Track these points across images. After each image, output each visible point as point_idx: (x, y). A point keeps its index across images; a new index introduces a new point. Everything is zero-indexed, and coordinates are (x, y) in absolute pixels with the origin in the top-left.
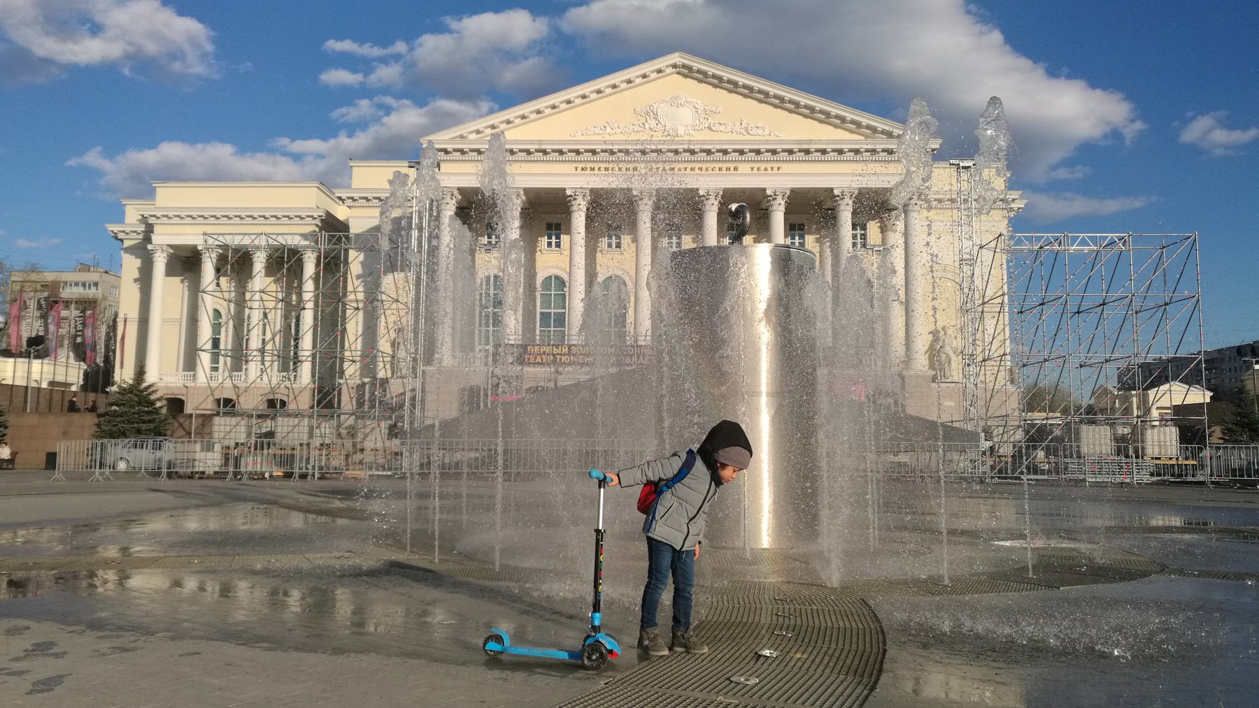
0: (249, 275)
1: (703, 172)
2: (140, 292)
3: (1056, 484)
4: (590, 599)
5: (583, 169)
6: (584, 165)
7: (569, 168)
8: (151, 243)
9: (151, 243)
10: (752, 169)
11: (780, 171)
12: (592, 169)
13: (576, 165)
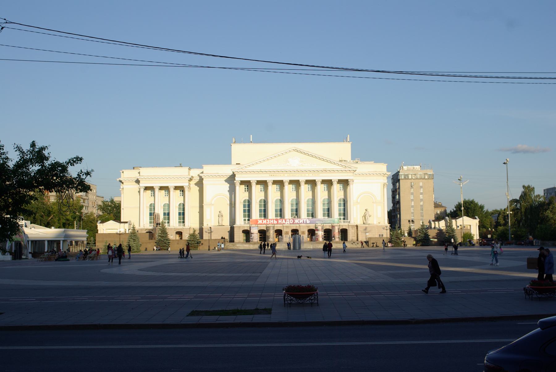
0: (267, 244)
1: (290, 176)
2: (230, 195)
3: (299, 252)
4: (208, 249)
5: (271, 175)
6: (273, 174)
7: (268, 175)
8: (235, 180)
9: (235, 180)
10: (313, 175)
11: (320, 175)
13: (313, 174)
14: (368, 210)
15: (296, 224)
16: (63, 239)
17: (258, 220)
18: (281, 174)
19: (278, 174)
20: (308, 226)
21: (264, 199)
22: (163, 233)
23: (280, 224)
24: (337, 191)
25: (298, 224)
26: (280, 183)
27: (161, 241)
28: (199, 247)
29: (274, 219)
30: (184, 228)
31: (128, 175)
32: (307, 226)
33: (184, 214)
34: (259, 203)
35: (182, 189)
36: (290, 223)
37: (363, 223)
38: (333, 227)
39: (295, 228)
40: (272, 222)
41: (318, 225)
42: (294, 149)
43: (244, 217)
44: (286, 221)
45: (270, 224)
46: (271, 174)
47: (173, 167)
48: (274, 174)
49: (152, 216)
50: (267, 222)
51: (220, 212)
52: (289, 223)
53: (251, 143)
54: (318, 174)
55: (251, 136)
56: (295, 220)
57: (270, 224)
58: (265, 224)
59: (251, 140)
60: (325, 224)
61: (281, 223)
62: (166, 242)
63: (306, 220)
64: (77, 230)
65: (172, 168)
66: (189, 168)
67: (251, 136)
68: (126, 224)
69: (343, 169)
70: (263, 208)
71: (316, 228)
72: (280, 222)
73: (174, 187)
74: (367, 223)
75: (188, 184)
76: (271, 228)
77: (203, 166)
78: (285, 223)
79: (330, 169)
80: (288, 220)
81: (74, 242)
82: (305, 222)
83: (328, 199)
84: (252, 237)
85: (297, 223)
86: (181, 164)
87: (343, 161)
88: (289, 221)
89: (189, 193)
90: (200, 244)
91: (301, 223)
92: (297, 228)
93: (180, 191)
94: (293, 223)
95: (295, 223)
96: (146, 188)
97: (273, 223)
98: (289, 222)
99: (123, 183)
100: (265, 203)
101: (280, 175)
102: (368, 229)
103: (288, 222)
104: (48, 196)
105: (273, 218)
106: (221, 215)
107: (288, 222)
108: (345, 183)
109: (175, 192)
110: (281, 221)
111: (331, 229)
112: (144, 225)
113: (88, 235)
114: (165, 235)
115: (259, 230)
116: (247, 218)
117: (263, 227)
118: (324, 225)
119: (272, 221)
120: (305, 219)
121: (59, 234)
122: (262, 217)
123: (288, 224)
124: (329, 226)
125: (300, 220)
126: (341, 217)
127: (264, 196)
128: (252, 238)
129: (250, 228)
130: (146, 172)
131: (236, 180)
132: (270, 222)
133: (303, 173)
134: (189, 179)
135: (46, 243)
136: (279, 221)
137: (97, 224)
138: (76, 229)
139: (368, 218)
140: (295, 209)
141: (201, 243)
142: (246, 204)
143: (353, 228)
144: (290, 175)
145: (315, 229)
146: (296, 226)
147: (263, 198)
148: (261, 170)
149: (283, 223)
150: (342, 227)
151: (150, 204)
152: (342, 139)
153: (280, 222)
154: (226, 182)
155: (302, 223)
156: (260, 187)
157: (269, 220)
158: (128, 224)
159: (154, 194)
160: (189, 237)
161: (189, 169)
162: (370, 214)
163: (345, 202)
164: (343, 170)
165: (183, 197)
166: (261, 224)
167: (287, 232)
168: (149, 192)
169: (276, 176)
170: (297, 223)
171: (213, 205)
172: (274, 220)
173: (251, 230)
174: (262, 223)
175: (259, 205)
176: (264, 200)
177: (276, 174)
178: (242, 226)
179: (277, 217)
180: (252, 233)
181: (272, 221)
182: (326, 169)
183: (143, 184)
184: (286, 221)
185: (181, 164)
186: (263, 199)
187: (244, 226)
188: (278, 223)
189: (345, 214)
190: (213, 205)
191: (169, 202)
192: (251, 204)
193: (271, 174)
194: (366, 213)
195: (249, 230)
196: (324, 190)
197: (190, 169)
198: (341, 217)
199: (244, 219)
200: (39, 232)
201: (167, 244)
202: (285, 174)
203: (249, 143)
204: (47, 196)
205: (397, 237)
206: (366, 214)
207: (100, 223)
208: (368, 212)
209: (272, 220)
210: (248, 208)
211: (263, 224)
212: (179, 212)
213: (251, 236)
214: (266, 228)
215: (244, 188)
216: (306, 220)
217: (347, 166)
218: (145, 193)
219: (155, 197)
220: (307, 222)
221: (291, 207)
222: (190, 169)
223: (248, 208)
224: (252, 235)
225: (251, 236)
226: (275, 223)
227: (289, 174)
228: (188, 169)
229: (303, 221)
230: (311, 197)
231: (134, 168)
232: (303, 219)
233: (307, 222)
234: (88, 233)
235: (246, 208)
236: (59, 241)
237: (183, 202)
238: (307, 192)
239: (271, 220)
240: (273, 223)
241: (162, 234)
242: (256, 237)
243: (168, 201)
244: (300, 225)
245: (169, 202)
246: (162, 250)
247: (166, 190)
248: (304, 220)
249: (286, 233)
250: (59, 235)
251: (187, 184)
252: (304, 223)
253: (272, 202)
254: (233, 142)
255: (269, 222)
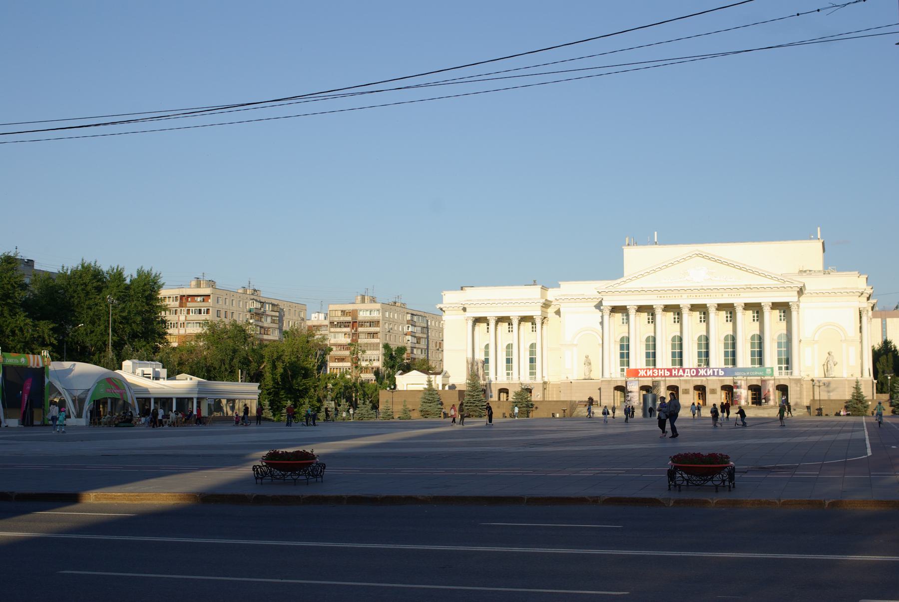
1: (691, 297)
8: (602, 306)
9: (602, 306)
12: (696, 296)
14: (833, 354)
15: (701, 376)
16: (196, 396)
17: (640, 371)
18: (683, 295)
19: (671, 295)
20: (722, 381)
21: (758, 333)
22: (475, 391)
23: (675, 376)
24: (773, 322)
25: (704, 376)
26: (729, 309)
27: (471, 403)
28: (531, 413)
29: (664, 369)
30: (791, 377)
31: (451, 298)
32: (719, 380)
33: (654, 354)
34: (671, 342)
35: (704, 310)
36: (691, 375)
37: (824, 376)
38: (763, 381)
39: (699, 384)
40: (661, 374)
41: (737, 378)
42: (697, 253)
43: (621, 366)
44: (684, 372)
45: (658, 376)
46: (659, 296)
47: (521, 285)
48: (666, 295)
49: (511, 364)
50: (653, 373)
51: (829, 353)
52: (689, 374)
53: (656, 244)
54: (738, 294)
55: (656, 233)
56: (700, 370)
57: (658, 376)
58: (650, 376)
59: (656, 241)
60: (751, 376)
61: (676, 375)
62: (478, 405)
63: (717, 370)
64: (242, 383)
65: (520, 287)
66: (543, 286)
67: (656, 233)
68: (438, 376)
69: (779, 284)
70: (730, 350)
71: (735, 383)
72: (675, 374)
73: (663, 307)
74: (830, 375)
75: (540, 312)
76: (662, 384)
77: (560, 283)
78: (683, 375)
79: (758, 285)
80: (689, 370)
81: (224, 402)
82: (716, 374)
83: (787, 335)
84: (629, 398)
85: (642, 375)
86: (535, 281)
87: (808, 272)
88: (689, 372)
89: (690, 317)
90: (534, 409)
91: (710, 375)
92: (703, 384)
93: (700, 313)
94: (697, 375)
95: (699, 374)
96: (615, 309)
97: (663, 375)
98: (690, 373)
99: (444, 311)
100: (759, 342)
101: (716, 296)
102: (833, 386)
103: (687, 373)
104: (356, 334)
105: (664, 368)
106: (588, 363)
107: (687, 373)
108: (784, 308)
109: (525, 326)
110: (676, 372)
111: (760, 385)
112: (611, 374)
113: (260, 391)
114: (476, 393)
115: (640, 386)
116: (784, 366)
117: (648, 382)
118: (748, 378)
119: (661, 371)
120: (716, 368)
121: (191, 389)
122: (755, 364)
123: (687, 376)
124: (757, 380)
125: (708, 370)
126: (509, 372)
127: (732, 329)
128: (629, 399)
129: (626, 382)
130: (473, 294)
131: (603, 305)
132: (658, 372)
133: (713, 293)
134: (542, 305)
135: (152, 401)
136: (673, 372)
137: (395, 376)
138: (241, 381)
139: (831, 367)
140: (704, 351)
141: (535, 406)
142: (728, 343)
143: (797, 384)
144: (690, 296)
145: (732, 385)
146: (702, 380)
147: (758, 333)
148: (702, 286)
149: (679, 375)
150: (779, 381)
151: (646, 337)
152: (804, 234)
153: (675, 374)
154: (596, 309)
155: (712, 374)
156: (726, 315)
157: (657, 371)
158: (442, 376)
159: (628, 319)
160: (514, 397)
161: (541, 288)
162: (836, 359)
163: (788, 341)
164: (779, 286)
165: (731, 323)
166: (644, 376)
167: (686, 390)
168: (619, 316)
169: (668, 298)
170: (702, 375)
171: (576, 345)
172: (666, 370)
173: (628, 387)
174: (645, 375)
175: (750, 344)
176: (705, 337)
177: (668, 295)
178: (613, 379)
179: (727, 365)
180: (629, 392)
181: (661, 371)
182: (750, 285)
183: (608, 303)
184: (684, 372)
185: (535, 281)
186: (757, 335)
187: (617, 380)
188: (671, 375)
189: (787, 362)
190: (576, 345)
191: (655, 333)
192: (764, 343)
193: (659, 296)
194: (828, 360)
195: (625, 386)
196: (779, 320)
197: (544, 288)
198: (509, 372)
199: (779, 367)
200: (164, 385)
201: (480, 407)
202: (682, 295)
203: (653, 244)
204: (354, 334)
205: (857, 400)
206: (828, 361)
207: (401, 374)
208: (832, 356)
209: (661, 369)
210: (732, 350)
211: (647, 377)
212: (507, 359)
213: (628, 396)
214: (653, 383)
215: (699, 316)
216: (717, 370)
217: (785, 280)
218: (638, 318)
219: (629, 325)
220: (720, 374)
221: (646, 350)
222: (544, 288)
223: (732, 350)
224: (630, 394)
225: (628, 396)
226: (666, 375)
227: (689, 295)
228: (540, 289)
229: (714, 372)
230: (785, 332)
231: (462, 289)
232: (713, 369)
233: (720, 374)
234: (259, 387)
235: (702, 349)
236: (192, 399)
237: (705, 334)
238: (777, 322)
239: (660, 370)
240: (663, 375)
241: (472, 392)
242: (774, 397)
243: (679, 330)
244: (708, 378)
245: (655, 333)
246: (473, 416)
247: (624, 313)
248: (714, 370)
249: (684, 391)
250: (191, 390)
251: (539, 313)
252: (714, 375)
253: (641, 341)
254: (627, 244)
255: (656, 373)
